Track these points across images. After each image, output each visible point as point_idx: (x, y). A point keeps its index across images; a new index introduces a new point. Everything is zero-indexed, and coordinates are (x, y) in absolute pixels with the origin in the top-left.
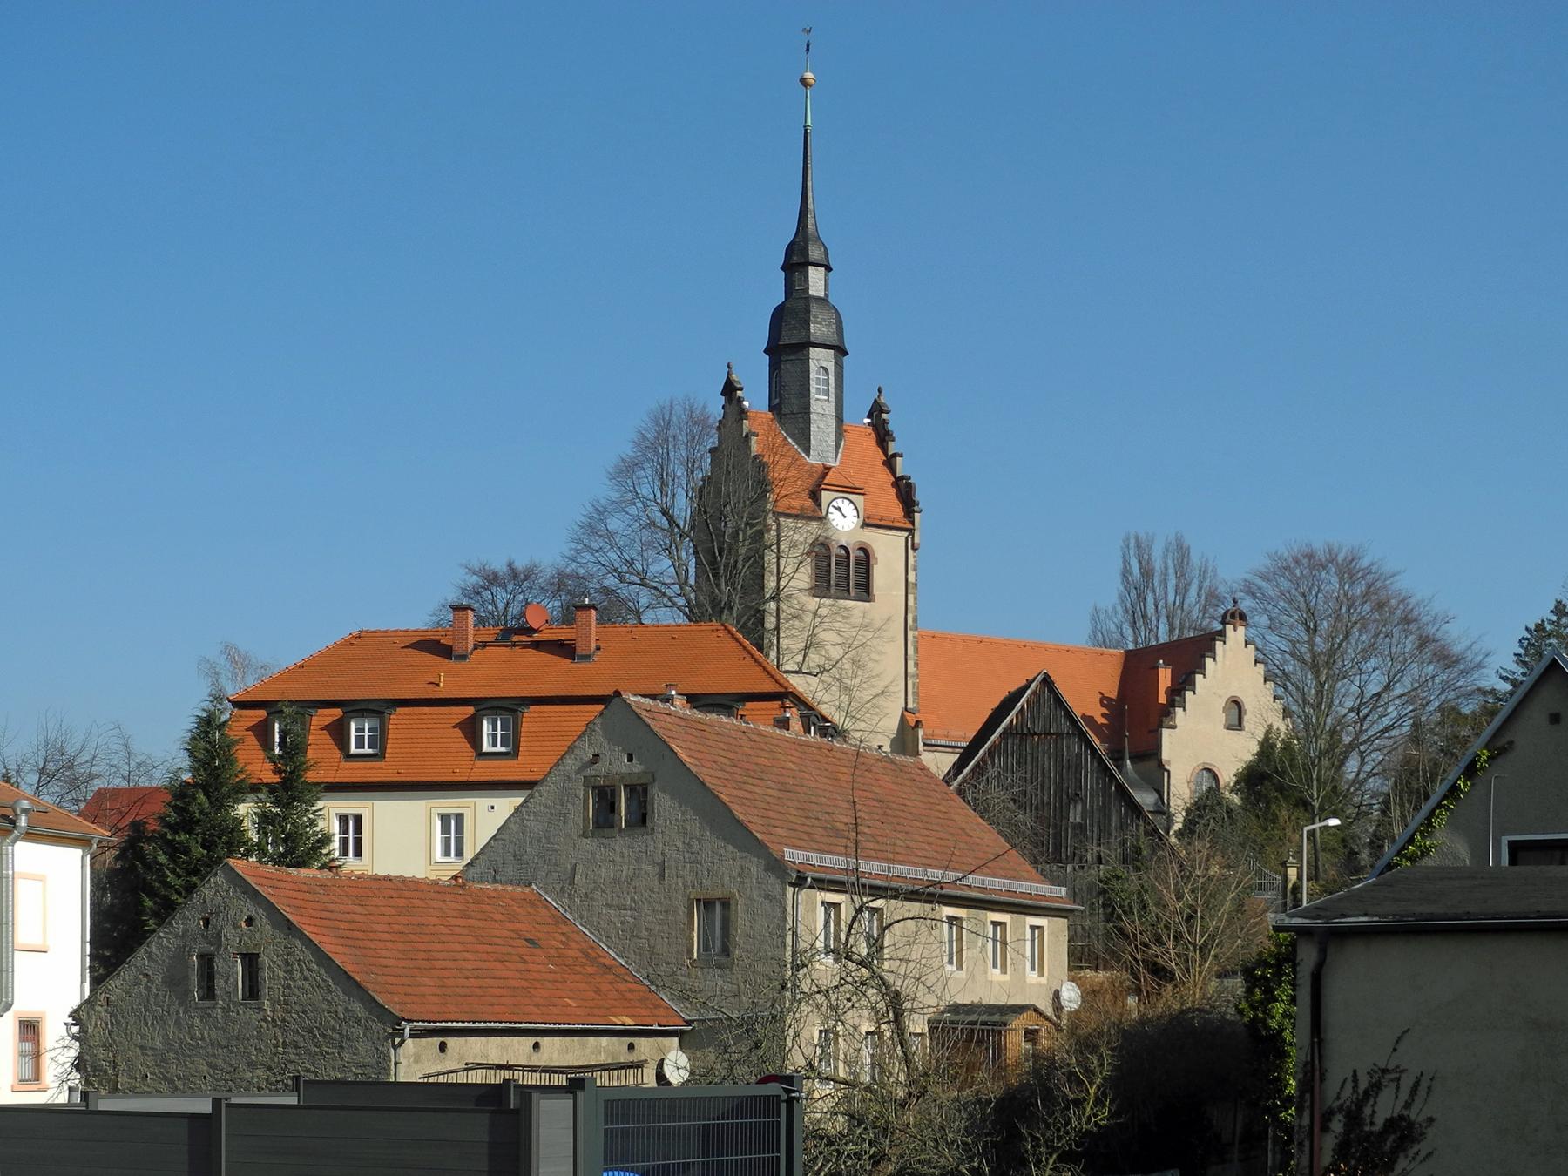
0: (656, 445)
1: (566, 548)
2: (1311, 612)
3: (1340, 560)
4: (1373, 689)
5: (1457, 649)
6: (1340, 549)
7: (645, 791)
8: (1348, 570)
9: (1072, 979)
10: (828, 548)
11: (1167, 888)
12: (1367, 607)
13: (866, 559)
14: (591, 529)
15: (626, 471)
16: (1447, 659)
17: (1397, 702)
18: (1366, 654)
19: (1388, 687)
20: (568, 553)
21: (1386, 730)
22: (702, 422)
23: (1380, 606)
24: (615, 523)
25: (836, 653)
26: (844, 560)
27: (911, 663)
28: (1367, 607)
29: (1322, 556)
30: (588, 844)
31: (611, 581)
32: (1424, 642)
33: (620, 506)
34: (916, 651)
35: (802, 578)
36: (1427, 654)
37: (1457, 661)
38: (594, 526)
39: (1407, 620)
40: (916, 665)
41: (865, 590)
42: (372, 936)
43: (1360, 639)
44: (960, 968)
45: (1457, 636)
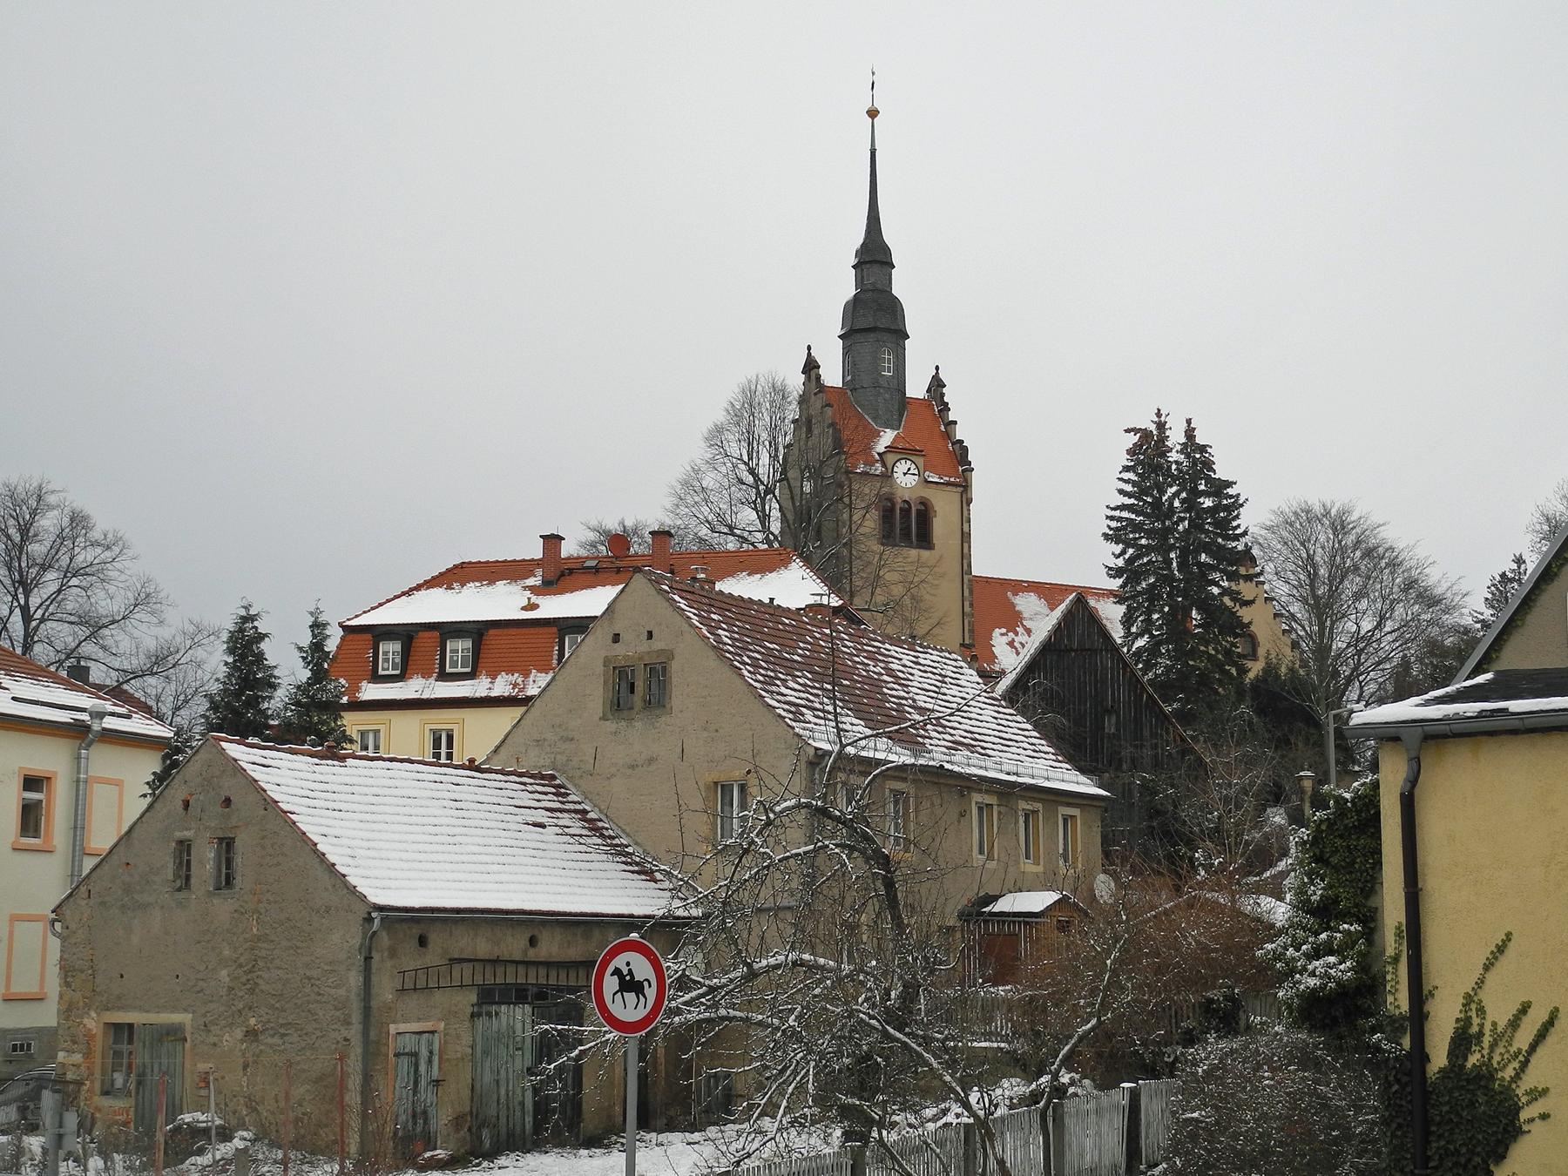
0: (746, 409)
1: (669, 502)
2: (1310, 558)
3: (1333, 512)
4: (1367, 625)
5: (1438, 591)
6: (1333, 503)
7: (664, 669)
8: (1339, 526)
9: (1105, 872)
10: (893, 505)
11: (685, 1004)
12: (1358, 554)
13: (925, 514)
14: (686, 484)
15: (716, 437)
16: (1430, 600)
17: (1390, 638)
18: (1358, 596)
19: (1379, 626)
20: (669, 506)
21: (1379, 663)
22: (780, 392)
23: (1368, 553)
24: (709, 481)
25: (897, 591)
26: (906, 512)
27: (967, 604)
28: (1358, 554)
29: (1318, 509)
30: (610, 726)
31: (704, 531)
32: (1410, 584)
33: (711, 463)
34: (971, 592)
35: (870, 523)
36: (1413, 594)
37: (1439, 602)
38: (691, 485)
39: (1394, 565)
40: (971, 605)
41: (925, 539)
42: (504, 825)
43: (1351, 585)
44: (990, 857)
45: (1436, 578)
